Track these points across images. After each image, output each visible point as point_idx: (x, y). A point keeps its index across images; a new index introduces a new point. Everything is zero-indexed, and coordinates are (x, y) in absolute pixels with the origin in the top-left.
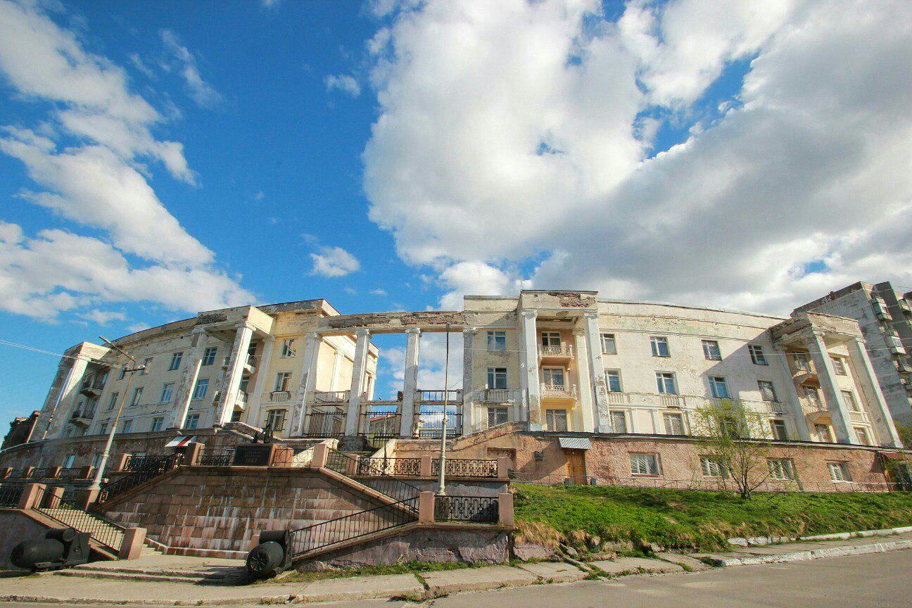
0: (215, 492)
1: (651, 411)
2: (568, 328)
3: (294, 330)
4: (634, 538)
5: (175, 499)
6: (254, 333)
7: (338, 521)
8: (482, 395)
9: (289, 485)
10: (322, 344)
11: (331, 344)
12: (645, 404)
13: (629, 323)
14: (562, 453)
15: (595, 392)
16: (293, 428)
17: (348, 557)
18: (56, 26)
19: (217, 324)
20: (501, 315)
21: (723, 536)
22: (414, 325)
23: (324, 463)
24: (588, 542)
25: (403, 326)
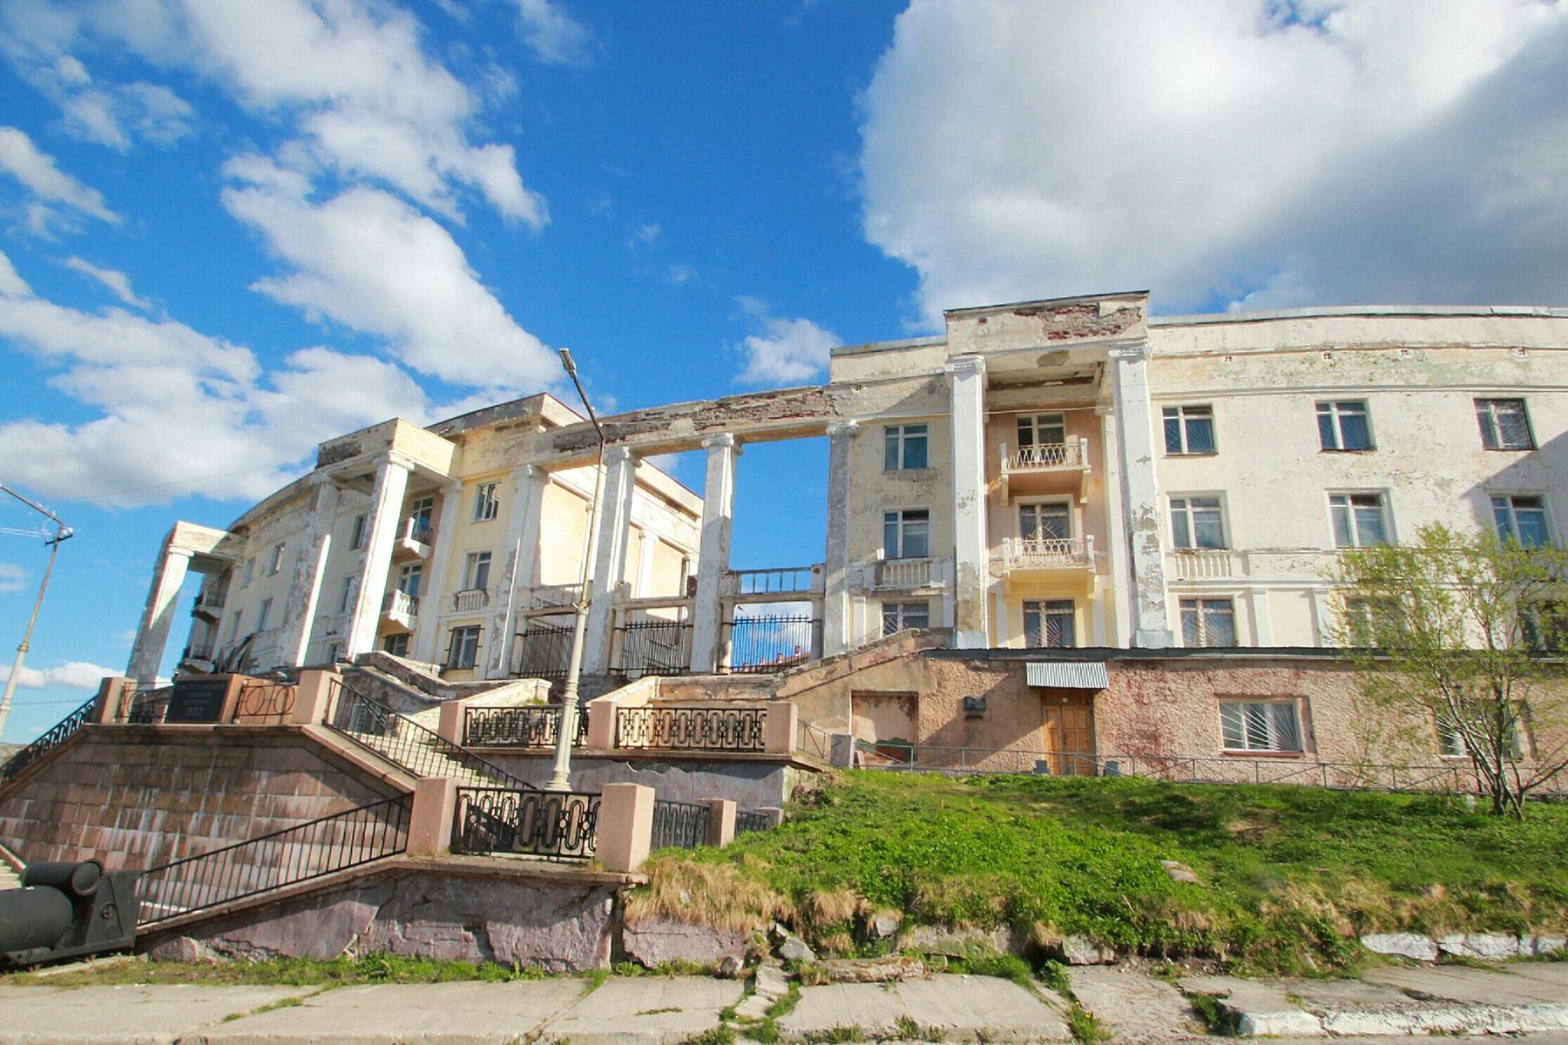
0: (135, 780)
1: (1310, 594)
2: (1083, 398)
3: (495, 462)
4: (1014, 916)
5: (74, 794)
6: (411, 474)
7: (261, 843)
8: (869, 574)
9: (248, 765)
10: (549, 490)
11: (573, 488)
12: (1295, 575)
13: (1254, 370)
14: (1035, 700)
15: (1131, 547)
16: (492, 663)
17: (247, 933)
18: (1067, 372)
19: (348, 462)
20: (916, 385)
21: (1344, 925)
22: (721, 428)
23: (318, 715)
24: (860, 929)
25: (696, 433)
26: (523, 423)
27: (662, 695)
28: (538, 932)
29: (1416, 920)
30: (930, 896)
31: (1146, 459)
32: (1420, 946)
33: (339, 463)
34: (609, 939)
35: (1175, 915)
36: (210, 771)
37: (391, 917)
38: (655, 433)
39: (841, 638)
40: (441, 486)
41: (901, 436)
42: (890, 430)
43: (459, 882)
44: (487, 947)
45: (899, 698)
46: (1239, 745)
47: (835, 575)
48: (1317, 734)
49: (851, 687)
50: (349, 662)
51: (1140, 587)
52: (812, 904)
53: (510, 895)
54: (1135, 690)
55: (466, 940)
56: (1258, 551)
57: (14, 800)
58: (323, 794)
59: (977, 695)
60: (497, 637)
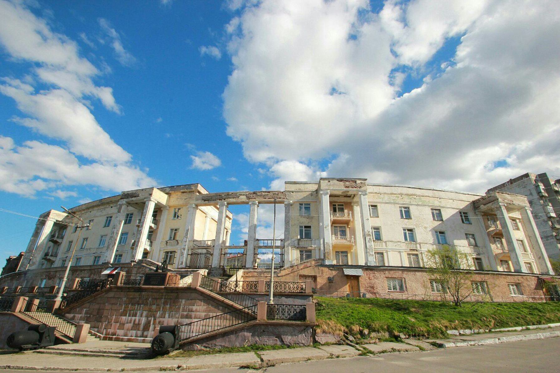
1: (400, 252)
4: (389, 330)
5: (108, 306)
7: (208, 320)
8: (296, 242)
9: (177, 298)
10: (198, 211)
12: (397, 248)
14: (345, 278)
16: (180, 263)
17: (214, 342)
19: (133, 199)
21: (444, 329)
22: (254, 200)
24: (361, 333)
26: (191, 192)
27: (244, 275)
28: (295, 337)
29: (455, 327)
30: (374, 326)
31: (368, 219)
32: (456, 332)
33: (130, 199)
34: (312, 338)
35: (417, 328)
36: (163, 299)
37: (255, 336)
38: (234, 199)
39: (289, 259)
40: (162, 207)
41: (303, 206)
42: (301, 204)
43: (272, 327)
44: (282, 341)
45: (311, 277)
46: (391, 289)
47: (287, 242)
48: (407, 287)
49: (299, 274)
50: (135, 262)
51: (368, 250)
52: (351, 328)
53: (286, 329)
54: (368, 276)
55: (276, 340)
56: (389, 241)
57: (78, 309)
58: (204, 306)
59: (331, 276)
60: (182, 255)
